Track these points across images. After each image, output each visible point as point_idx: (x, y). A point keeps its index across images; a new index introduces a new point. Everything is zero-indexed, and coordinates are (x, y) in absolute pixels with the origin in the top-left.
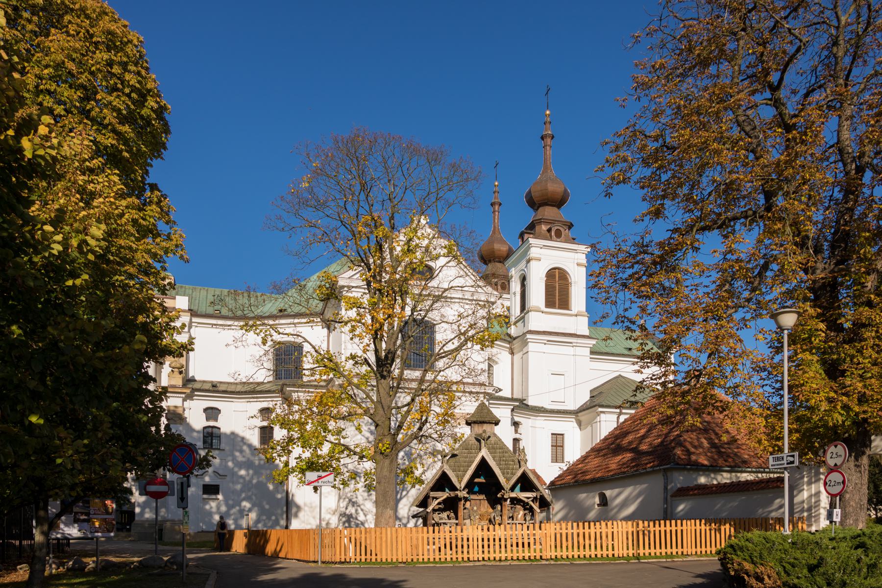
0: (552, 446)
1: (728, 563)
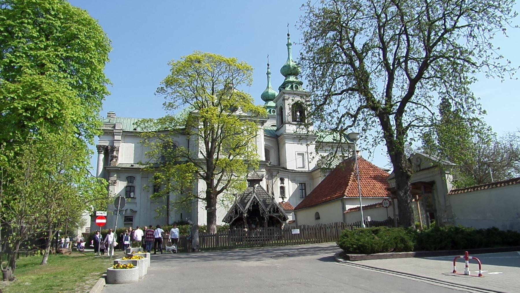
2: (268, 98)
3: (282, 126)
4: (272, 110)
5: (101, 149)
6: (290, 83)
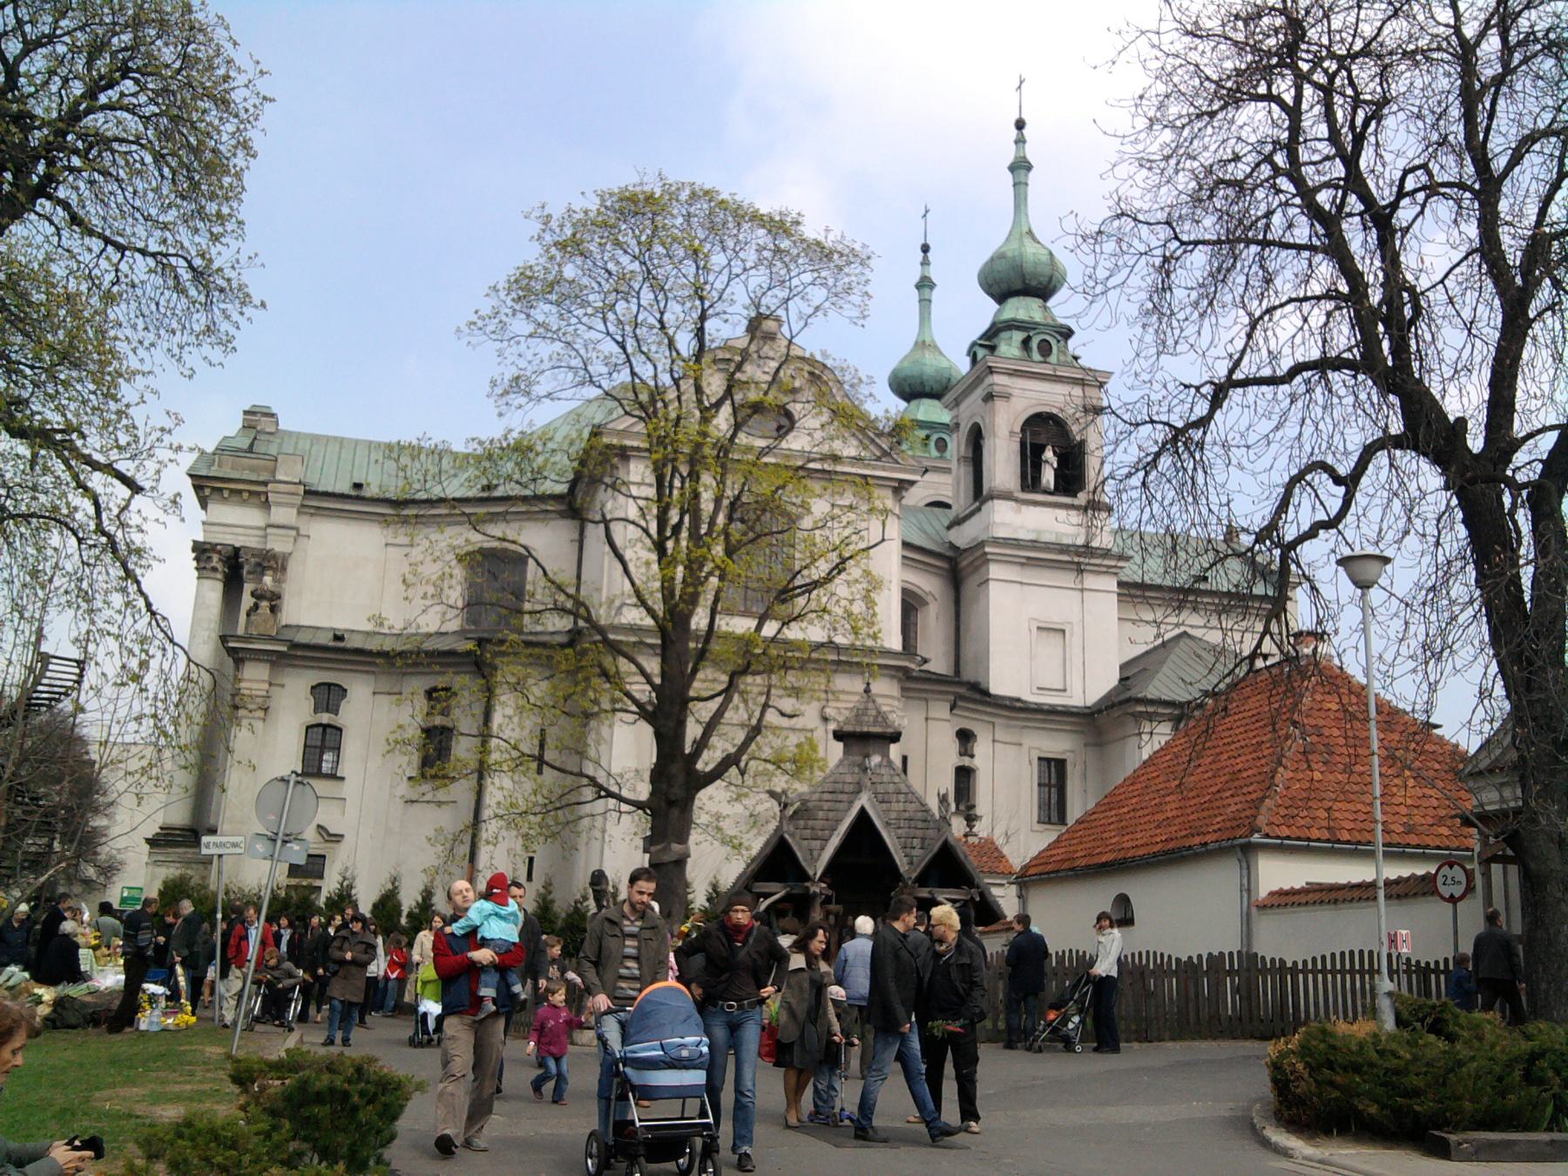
0: (1040, 785)
1: (168, 980)
2: (919, 389)
3: (979, 509)
4: (934, 437)
5: (215, 557)
6: (1018, 328)
